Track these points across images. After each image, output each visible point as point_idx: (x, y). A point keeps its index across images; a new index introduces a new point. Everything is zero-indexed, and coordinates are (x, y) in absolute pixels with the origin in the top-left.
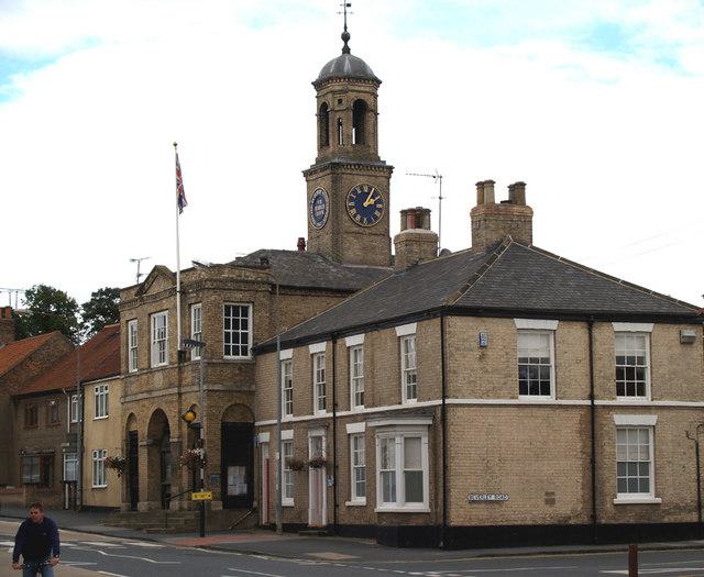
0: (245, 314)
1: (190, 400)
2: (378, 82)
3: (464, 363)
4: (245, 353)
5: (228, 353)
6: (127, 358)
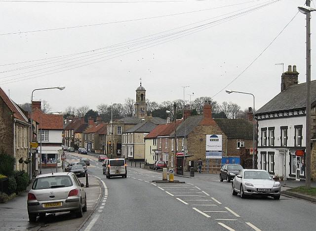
3: (136, 139)
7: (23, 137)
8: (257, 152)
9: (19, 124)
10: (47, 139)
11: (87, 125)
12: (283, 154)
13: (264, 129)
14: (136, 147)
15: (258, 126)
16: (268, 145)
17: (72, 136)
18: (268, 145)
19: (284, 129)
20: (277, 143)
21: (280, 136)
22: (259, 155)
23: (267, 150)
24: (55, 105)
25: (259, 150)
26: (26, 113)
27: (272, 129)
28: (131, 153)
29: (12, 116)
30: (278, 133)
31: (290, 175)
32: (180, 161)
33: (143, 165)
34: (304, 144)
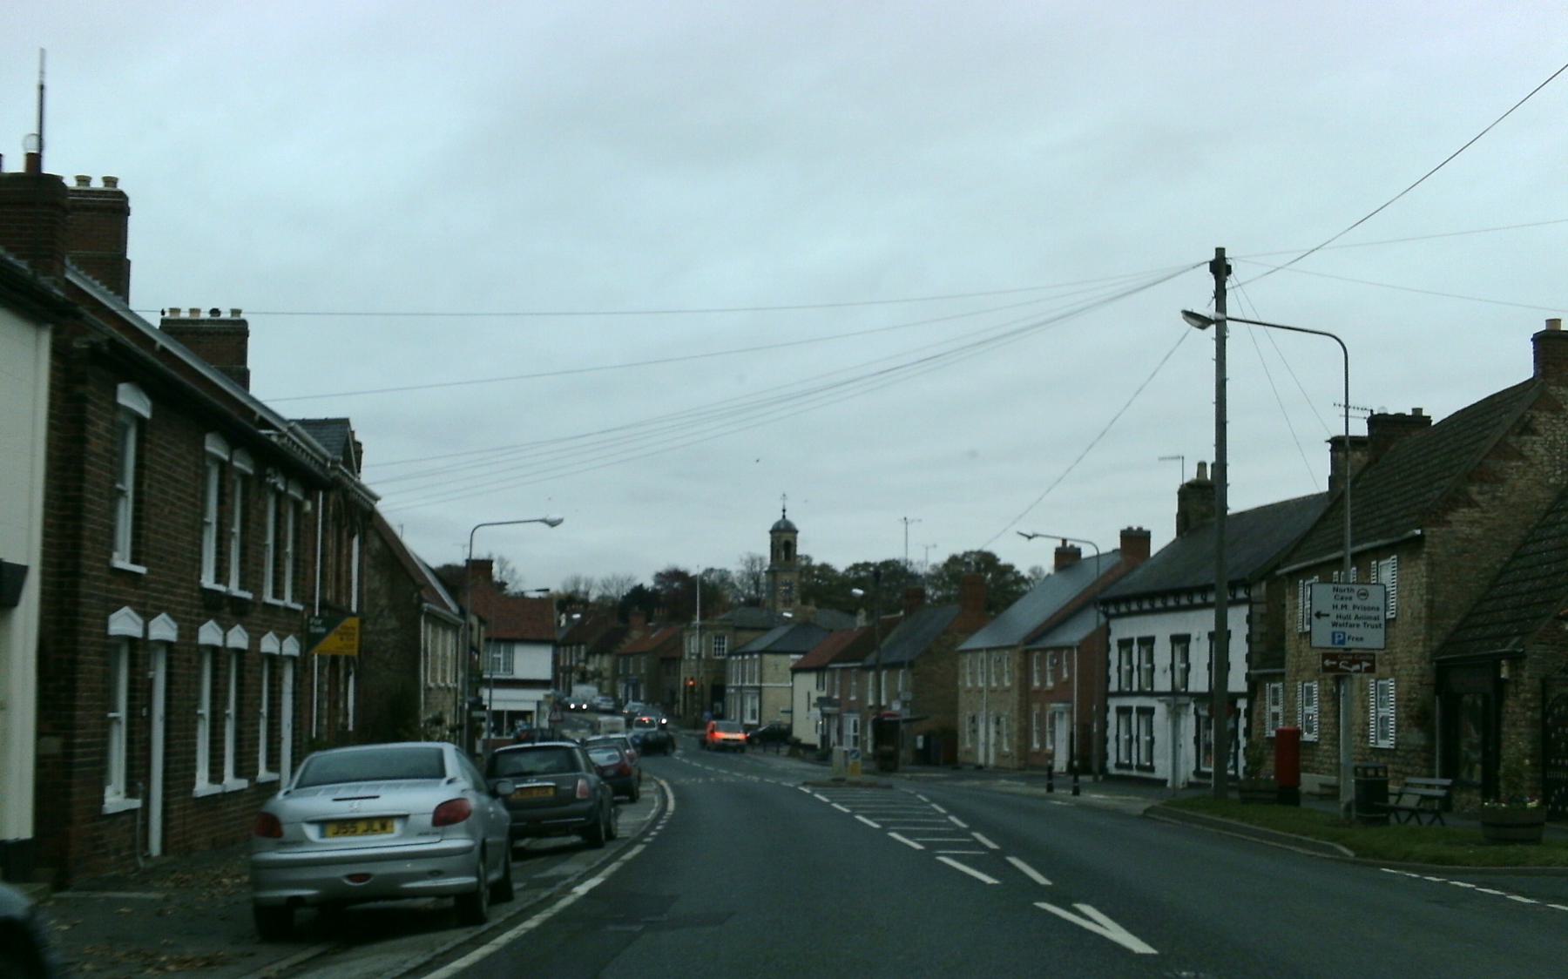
0: (724, 638)
1: (701, 674)
2: (796, 532)
3: (769, 671)
4: (723, 654)
5: (715, 655)
6: (91, 201)
7: (444, 655)
8: (1107, 709)
9: (437, 620)
10: (509, 667)
11: (624, 633)
12: (1175, 714)
13: (1125, 644)
14: (769, 698)
15: (1108, 632)
16: (1135, 688)
17: (582, 665)
18: (1135, 688)
19: (1181, 642)
20: (1163, 683)
21: (1169, 661)
22: (1112, 717)
23: (1135, 702)
24: (1247, 671)
25: (1113, 704)
26: (453, 591)
27: (1147, 642)
28: (753, 712)
29: (416, 595)
30: (1163, 653)
31: (1197, 773)
32: (885, 729)
33: (785, 750)
34: (1237, 682)
